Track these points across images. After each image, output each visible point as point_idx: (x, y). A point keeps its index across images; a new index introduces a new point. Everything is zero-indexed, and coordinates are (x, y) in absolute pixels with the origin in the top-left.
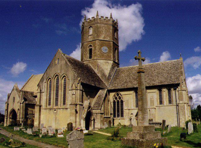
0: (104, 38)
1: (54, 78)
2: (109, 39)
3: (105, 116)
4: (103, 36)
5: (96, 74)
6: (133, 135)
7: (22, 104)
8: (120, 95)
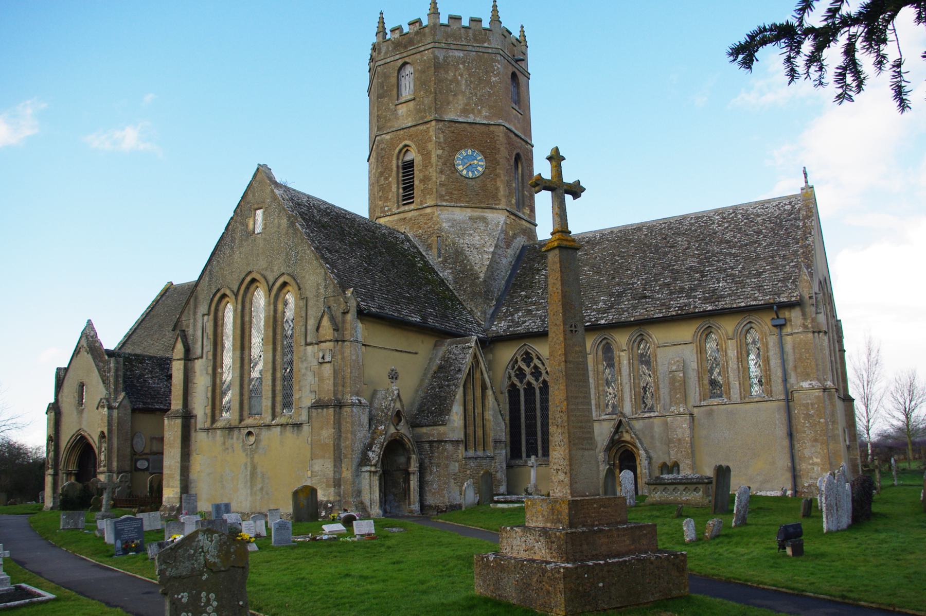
0: (465, 112)
1: (242, 292)
2: (486, 117)
3: (471, 453)
4: (461, 101)
5: (432, 270)
6: (523, 539)
7: (115, 412)
8: (536, 361)
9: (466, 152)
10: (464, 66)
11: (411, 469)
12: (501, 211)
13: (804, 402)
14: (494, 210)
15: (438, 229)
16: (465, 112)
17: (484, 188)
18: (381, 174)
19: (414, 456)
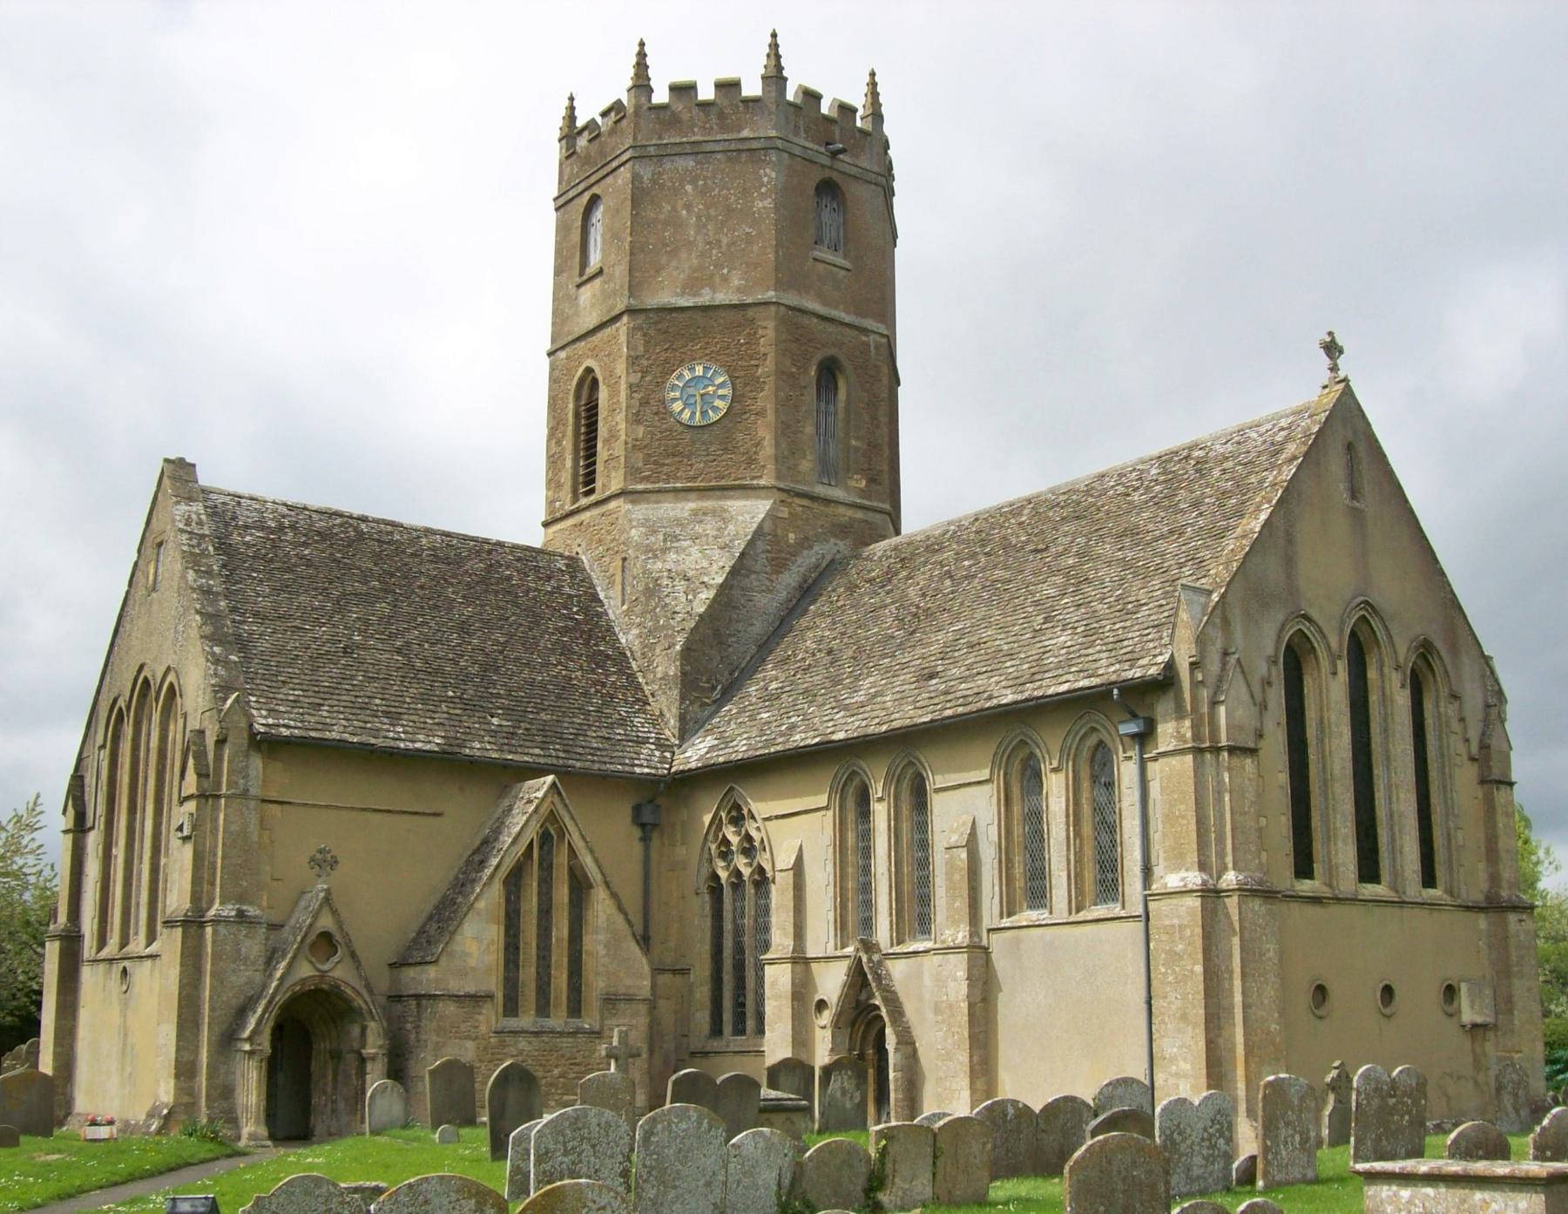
0: (692, 286)
2: (739, 290)
9: (692, 369)
10: (696, 187)
11: (369, 1050)
12: (765, 491)
13: (1167, 923)
14: (749, 492)
15: (623, 543)
16: (692, 286)
19: (372, 1025)
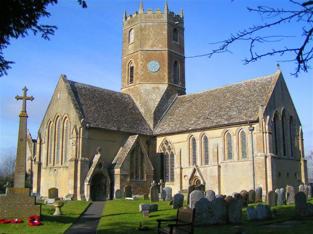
0: (152, 46)
2: (161, 48)
4: (151, 42)
5: (137, 109)
8: (169, 144)
17: (159, 76)
18: (123, 72)
